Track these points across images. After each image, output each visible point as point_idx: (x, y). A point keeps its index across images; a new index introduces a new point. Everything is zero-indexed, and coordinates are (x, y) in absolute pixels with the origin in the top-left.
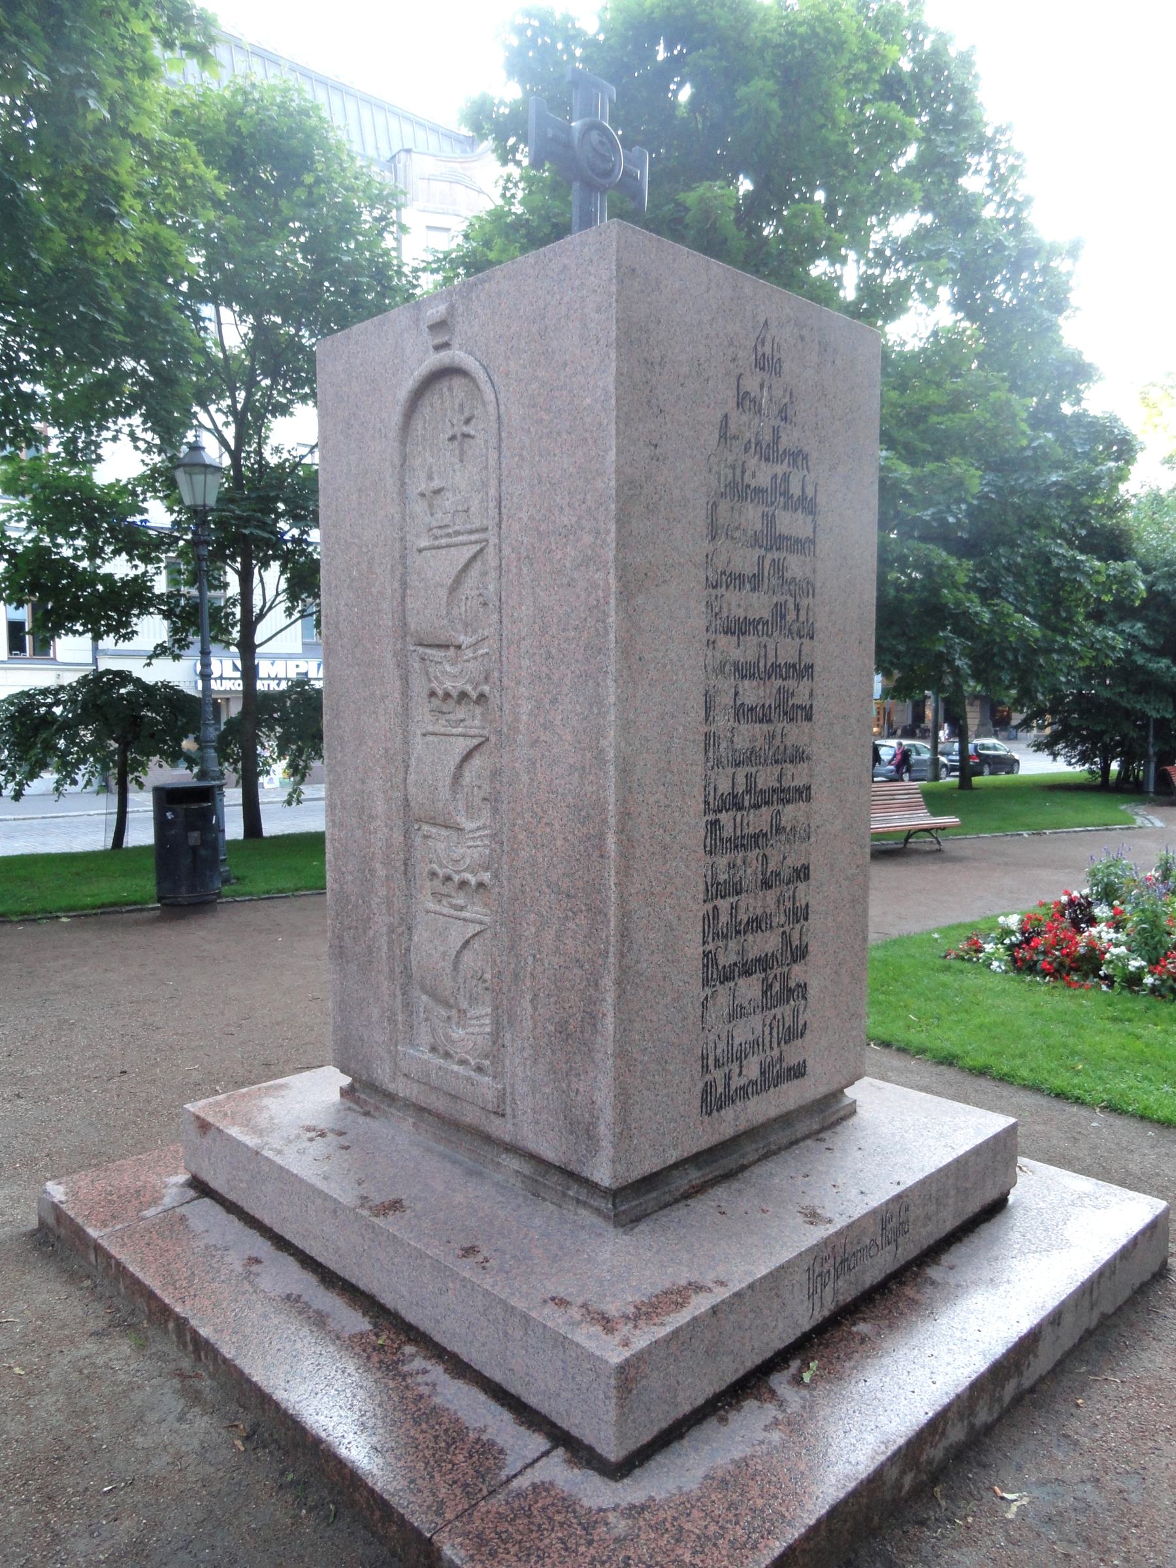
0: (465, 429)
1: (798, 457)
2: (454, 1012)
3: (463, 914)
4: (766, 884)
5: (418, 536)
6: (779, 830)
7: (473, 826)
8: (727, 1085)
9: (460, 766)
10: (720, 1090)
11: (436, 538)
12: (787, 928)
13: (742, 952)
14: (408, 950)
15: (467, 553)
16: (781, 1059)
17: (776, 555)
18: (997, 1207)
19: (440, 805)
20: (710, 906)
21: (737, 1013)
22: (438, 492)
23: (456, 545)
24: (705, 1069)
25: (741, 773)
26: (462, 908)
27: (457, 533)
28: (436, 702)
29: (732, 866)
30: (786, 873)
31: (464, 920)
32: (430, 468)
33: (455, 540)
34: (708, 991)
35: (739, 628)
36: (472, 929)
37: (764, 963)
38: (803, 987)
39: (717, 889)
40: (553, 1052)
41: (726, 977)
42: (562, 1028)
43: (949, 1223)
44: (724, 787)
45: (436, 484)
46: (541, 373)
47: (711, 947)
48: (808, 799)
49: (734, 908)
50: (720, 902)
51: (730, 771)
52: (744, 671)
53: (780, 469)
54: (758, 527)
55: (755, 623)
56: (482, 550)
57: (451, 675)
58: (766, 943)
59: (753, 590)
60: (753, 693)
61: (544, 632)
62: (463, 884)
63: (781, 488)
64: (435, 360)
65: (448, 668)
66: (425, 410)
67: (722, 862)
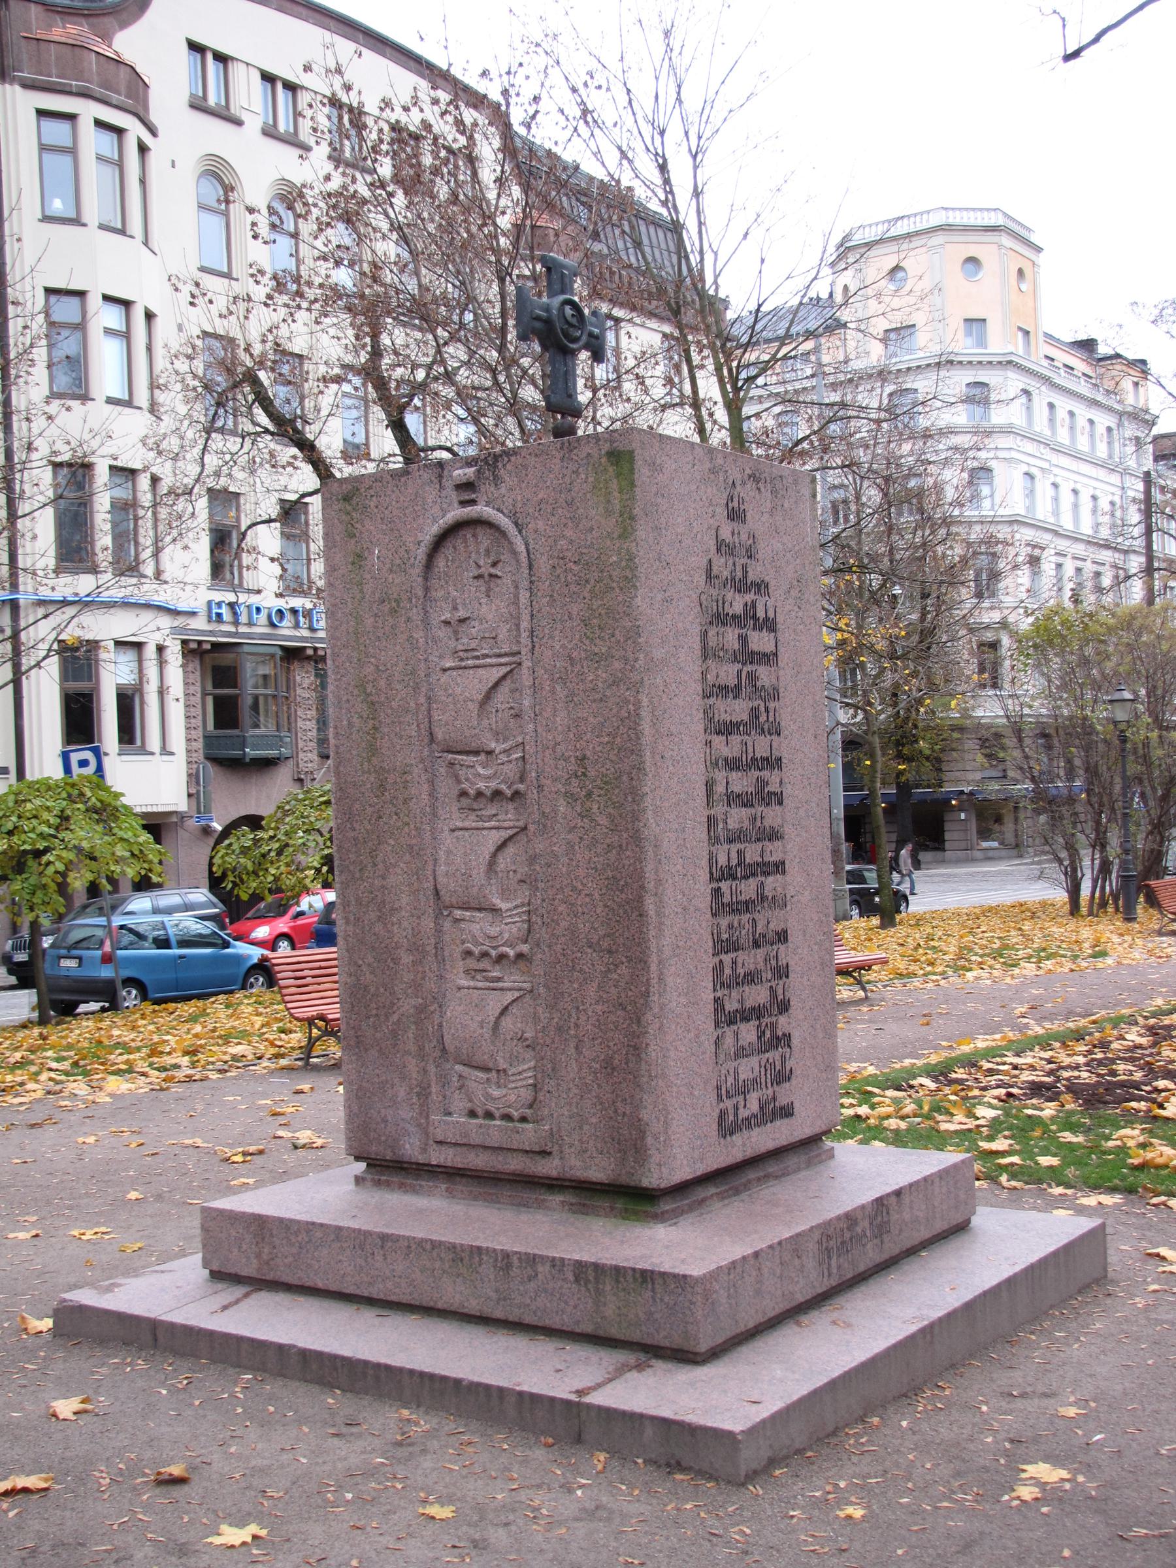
0: (493, 571)
1: (761, 587)
2: (494, 1074)
3: (500, 984)
4: (757, 945)
5: (441, 657)
6: (763, 898)
7: (509, 905)
8: (736, 1114)
9: (494, 855)
10: (731, 1118)
11: (462, 660)
12: (773, 984)
13: (741, 1001)
14: (440, 1026)
15: (497, 673)
16: (774, 1099)
17: (749, 668)
18: (962, 1228)
19: (475, 890)
20: (716, 960)
21: (741, 1053)
22: (462, 621)
23: (484, 666)
24: (719, 1097)
25: (735, 848)
26: (499, 979)
27: (486, 656)
28: (465, 802)
29: (731, 926)
30: (770, 935)
31: (502, 989)
32: (454, 600)
33: (477, 662)
34: (720, 1031)
35: (727, 729)
36: (510, 996)
37: (757, 1013)
38: (787, 1036)
39: (723, 946)
40: (599, 1086)
41: (732, 1022)
42: (608, 1066)
43: (925, 1234)
44: (722, 861)
45: (462, 614)
46: (569, 533)
47: (719, 994)
48: (784, 872)
49: (734, 962)
50: (723, 957)
51: (726, 847)
52: (733, 765)
53: (749, 597)
54: (736, 646)
55: (738, 724)
56: (511, 671)
57: (481, 776)
58: (757, 995)
59: (735, 698)
60: (741, 783)
61: (579, 737)
62: (502, 957)
63: (750, 612)
64: (457, 513)
65: (481, 771)
66: (447, 551)
67: (724, 922)
